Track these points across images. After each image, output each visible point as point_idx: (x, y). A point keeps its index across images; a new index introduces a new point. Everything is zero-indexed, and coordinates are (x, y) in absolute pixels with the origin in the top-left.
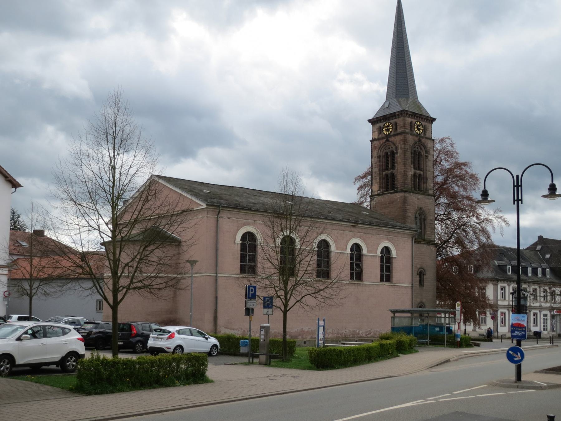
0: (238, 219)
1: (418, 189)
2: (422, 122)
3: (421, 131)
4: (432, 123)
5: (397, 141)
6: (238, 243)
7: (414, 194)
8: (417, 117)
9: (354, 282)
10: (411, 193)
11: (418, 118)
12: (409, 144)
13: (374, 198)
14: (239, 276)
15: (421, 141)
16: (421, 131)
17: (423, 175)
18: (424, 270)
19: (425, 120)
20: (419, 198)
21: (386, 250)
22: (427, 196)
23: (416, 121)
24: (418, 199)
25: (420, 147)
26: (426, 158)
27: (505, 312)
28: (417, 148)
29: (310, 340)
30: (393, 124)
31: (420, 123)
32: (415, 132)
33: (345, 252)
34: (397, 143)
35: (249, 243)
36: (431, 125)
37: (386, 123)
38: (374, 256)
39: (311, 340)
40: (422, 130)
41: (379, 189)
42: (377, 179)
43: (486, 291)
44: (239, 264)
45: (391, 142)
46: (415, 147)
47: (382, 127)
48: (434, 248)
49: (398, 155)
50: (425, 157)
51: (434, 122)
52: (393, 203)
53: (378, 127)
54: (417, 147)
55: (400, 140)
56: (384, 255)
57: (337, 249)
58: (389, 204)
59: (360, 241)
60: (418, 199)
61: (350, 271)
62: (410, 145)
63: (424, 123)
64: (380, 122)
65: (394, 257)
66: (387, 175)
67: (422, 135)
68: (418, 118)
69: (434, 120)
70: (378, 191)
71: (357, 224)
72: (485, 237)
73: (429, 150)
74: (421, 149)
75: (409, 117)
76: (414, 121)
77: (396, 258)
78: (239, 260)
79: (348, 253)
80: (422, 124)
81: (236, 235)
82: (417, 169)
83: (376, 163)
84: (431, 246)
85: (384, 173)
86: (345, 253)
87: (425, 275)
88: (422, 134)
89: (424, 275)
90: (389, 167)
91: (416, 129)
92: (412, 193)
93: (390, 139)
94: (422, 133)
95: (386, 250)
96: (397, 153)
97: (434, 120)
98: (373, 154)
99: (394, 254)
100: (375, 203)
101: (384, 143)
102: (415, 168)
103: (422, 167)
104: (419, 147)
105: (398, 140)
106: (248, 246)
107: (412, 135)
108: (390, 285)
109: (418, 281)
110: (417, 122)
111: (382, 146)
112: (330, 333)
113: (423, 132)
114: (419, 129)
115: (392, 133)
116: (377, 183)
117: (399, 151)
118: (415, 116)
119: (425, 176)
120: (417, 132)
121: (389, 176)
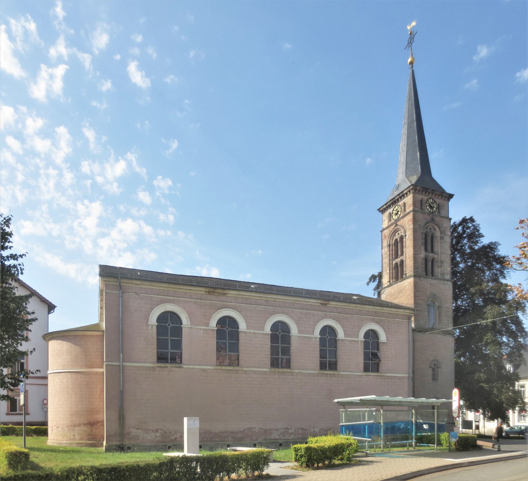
0: (151, 296)
1: (431, 275)
2: (435, 199)
3: (435, 209)
4: (449, 200)
5: (405, 223)
6: (152, 326)
7: (426, 279)
8: (429, 193)
9: (326, 372)
10: (422, 278)
11: (430, 195)
12: (419, 223)
13: (384, 291)
14: (154, 365)
15: (435, 220)
16: (435, 209)
17: (438, 258)
18: (439, 363)
19: (440, 197)
20: (432, 283)
21: (372, 335)
22: (442, 281)
23: (429, 198)
24: (431, 284)
25: (433, 227)
26: (441, 239)
27: (188, 453)
28: (430, 229)
29: (262, 442)
30: (402, 206)
31: (433, 200)
32: (426, 210)
33: (312, 336)
34: (405, 226)
35: (278, 333)
36: (446, 202)
37: (395, 207)
38: (354, 341)
39: (263, 442)
40: (436, 208)
41: (389, 280)
42: (387, 270)
43: (525, 389)
44: (155, 351)
45: (400, 226)
46: (427, 228)
47: (391, 213)
48: (451, 339)
49: (407, 237)
50: (439, 238)
51: (451, 200)
52: (402, 292)
53: (388, 215)
54: (429, 227)
55: (409, 221)
56: (370, 340)
57: (300, 332)
58: (398, 293)
59: (334, 323)
60: (431, 284)
61: (319, 359)
62: (421, 225)
63: (438, 201)
64: (390, 208)
65: (383, 343)
66: (397, 264)
67: (436, 213)
68: (430, 195)
69: (451, 196)
70: (388, 282)
71: (328, 301)
72: (489, 275)
73: (445, 230)
74: (435, 229)
75: (419, 194)
76: (425, 198)
77: (385, 343)
78: (155, 346)
79: (316, 338)
80: (435, 202)
81: (149, 316)
82: (430, 252)
83: (386, 254)
84: (447, 336)
85: (394, 262)
86: (312, 338)
87: (440, 367)
88: (436, 212)
89: (438, 368)
90: (399, 254)
91: (428, 207)
92: (423, 277)
93: (399, 223)
94: (435, 211)
95: (372, 335)
96: (406, 236)
97: (451, 196)
98: (383, 244)
99: (383, 337)
100: (385, 296)
101: (393, 229)
102: (426, 250)
103: (436, 250)
104: (432, 228)
105: (407, 221)
106: (170, 329)
107: (421, 213)
108: (378, 376)
109: (431, 375)
110: (430, 199)
111: (391, 233)
112: (292, 433)
113: (437, 211)
114: (431, 207)
115: (401, 216)
116: (387, 274)
117: (407, 234)
118: (426, 192)
119: (439, 259)
120: (429, 210)
121: (399, 264)
